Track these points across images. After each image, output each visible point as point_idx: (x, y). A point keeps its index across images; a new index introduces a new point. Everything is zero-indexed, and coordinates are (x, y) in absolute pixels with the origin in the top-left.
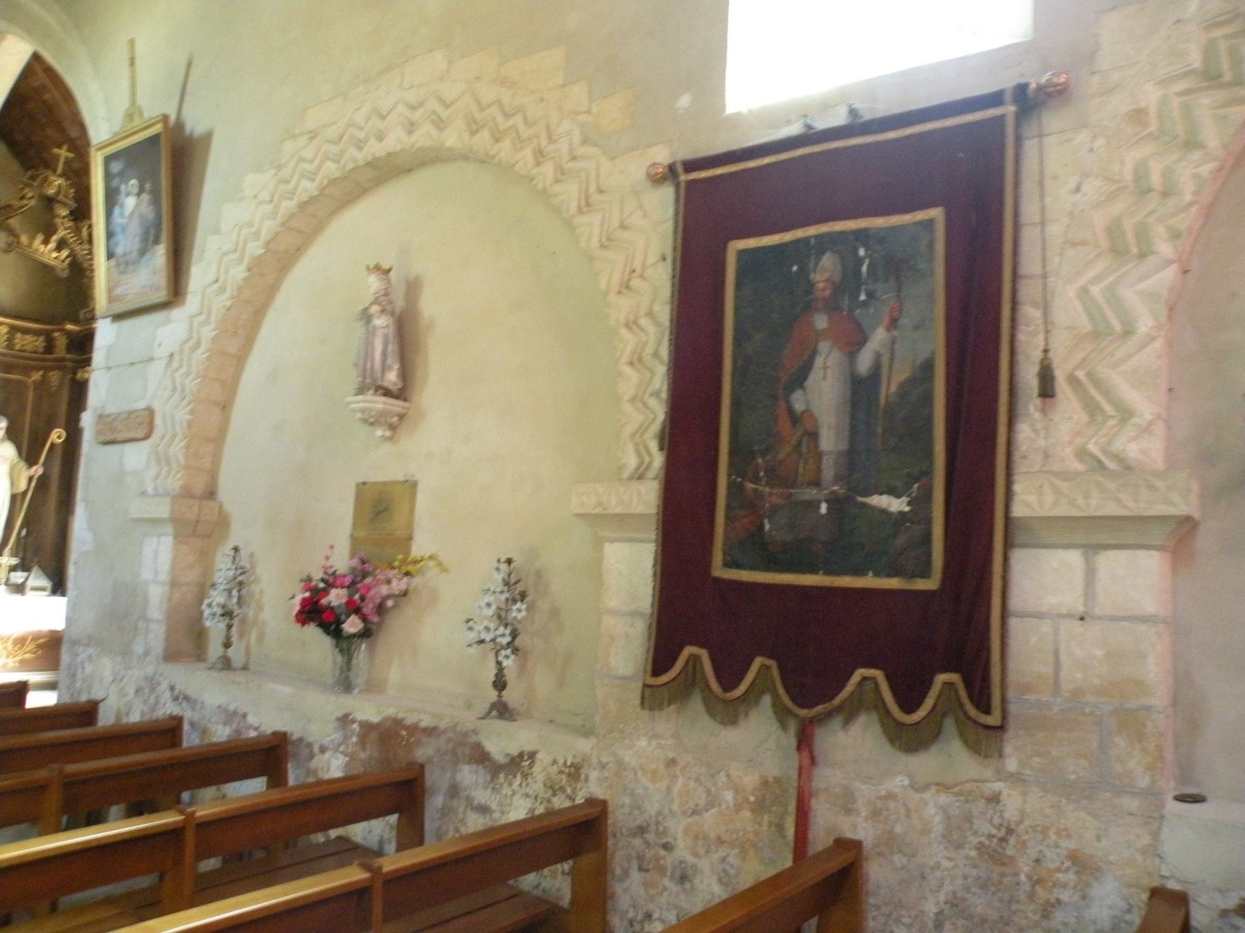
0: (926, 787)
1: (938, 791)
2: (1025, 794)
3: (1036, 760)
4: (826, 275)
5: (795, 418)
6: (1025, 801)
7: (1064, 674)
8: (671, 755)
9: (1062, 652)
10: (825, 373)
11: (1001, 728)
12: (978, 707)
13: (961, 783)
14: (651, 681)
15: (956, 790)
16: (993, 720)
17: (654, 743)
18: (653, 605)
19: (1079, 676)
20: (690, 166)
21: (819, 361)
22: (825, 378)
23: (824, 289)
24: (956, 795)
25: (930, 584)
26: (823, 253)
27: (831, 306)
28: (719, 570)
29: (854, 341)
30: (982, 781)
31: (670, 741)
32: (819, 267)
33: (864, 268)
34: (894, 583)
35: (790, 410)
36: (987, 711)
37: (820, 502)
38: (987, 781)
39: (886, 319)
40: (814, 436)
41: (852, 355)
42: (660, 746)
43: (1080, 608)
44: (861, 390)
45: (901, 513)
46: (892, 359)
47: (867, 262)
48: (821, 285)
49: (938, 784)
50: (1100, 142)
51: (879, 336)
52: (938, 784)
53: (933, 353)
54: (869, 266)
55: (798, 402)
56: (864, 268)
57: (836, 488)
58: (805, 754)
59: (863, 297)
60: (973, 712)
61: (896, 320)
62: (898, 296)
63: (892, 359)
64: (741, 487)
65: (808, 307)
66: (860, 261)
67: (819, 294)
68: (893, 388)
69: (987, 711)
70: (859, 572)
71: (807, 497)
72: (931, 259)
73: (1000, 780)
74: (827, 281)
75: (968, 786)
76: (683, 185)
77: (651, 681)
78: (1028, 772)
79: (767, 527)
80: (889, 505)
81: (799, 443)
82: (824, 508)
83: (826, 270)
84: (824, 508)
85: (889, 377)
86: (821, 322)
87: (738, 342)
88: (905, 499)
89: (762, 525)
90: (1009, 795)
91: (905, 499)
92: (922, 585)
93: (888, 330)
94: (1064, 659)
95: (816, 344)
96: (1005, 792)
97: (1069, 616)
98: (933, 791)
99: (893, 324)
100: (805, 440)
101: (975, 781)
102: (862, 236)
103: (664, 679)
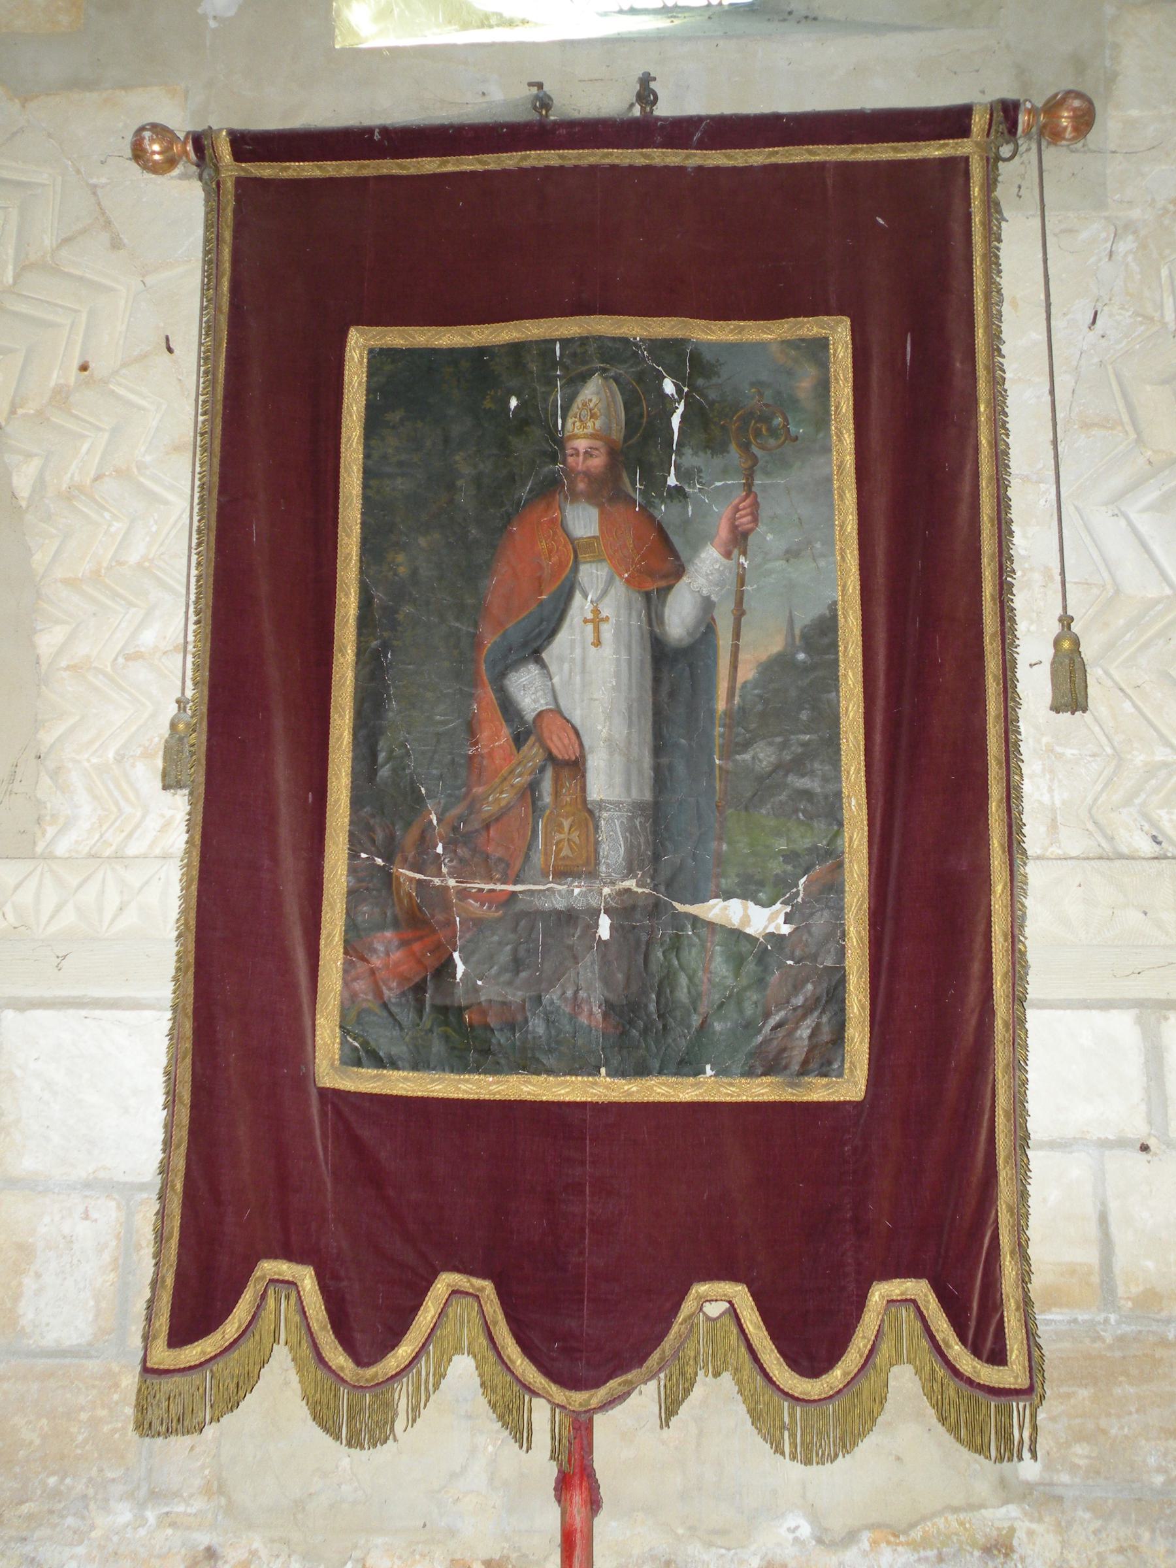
0: (851, 1537)
1: (875, 1543)
2: (1062, 1528)
3: (1081, 1449)
4: (591, 426)
5: (523, 732)
6: (1064, 1544)
7: (1121, 1262)
8: (204, 1539)
9: (1113, 1219)
10: (597, 631)
11: (1029, 1392)
12: (976, 1352)
13: (924, 1519)
14: (162, 1356)
15: (917, 1534)
16: (1011, 1375)
17: (151, 1515)
18: (165, 1168)
19: (1150, 1264)
20: (248, 145)
21: (580, 607)
22: (598, 643)
23: (588, 455)
24: (915, 1546)
25: (850, 1084)
26: (584, 378)
27: (606, 490)
28: (330, 1069)
29: (657, 564)
30: (972, 1507)
31: (198, 1504)
32: (575, 408)
33: (676, 421)
34: (761, 1090)
35: (508, 708)
36: (998, 1357)
37: (597, 913)
38: (982, 1506)
39: (723, 532)
40: (576, 767)
41: (653, 602)
42: (168, 1521)
43: (1138, 1129)
44: (672, 672)
45: (776, 939)
46: (739, 613)
47: (681, 408)
48: (582, 444)
49: (872, 1527)
50: (1125, 246)
51: (707, 567)
52: (872, 1527)
53: (833, 607)
54: (684, 416)
55: (528, 690)
56: (676, 421)
57: (631, 884)
58: (578, 1498)
59: (672, 481)
60: (967, 1363)
61: (745, 535)
62: (749, 486)
63: (739, 613)
64: (387, 878)
65: (550, 488)
66: (665, 406)
67: (577, 463)
68: (747, 673)
69: (998, 1357)
70: (688, 1066)
71: (560, 904)
72: (822, 421)
73: (1006, 1502)
74: (593, 436)
75: (940, 1522)
76: (229, 185)
77: (162, 1356)
78: (1065, 1478)
79: (460, 969)
80: (746, 919)
81: (533, 787)
82: (604, 929)
83: (588, 419)
84: (604, 929)
85: (735, 651)
86: (583, 521)
87: (371, 548)
88: (780, 909)
89: (450, 963)
90: (1031, 1533)
91: (780, 909)
92: (819, 1091)
93: (728, 555)
94: (1122, 1237)
95: (575, 570)
96: (1023, 1527)
97: (1121, 1143)
98: (865, 1545)
99: (739, 540)
100: (549, 774)
101: (955, 1510)
102: (672, 353)
103: (193, 1353)
